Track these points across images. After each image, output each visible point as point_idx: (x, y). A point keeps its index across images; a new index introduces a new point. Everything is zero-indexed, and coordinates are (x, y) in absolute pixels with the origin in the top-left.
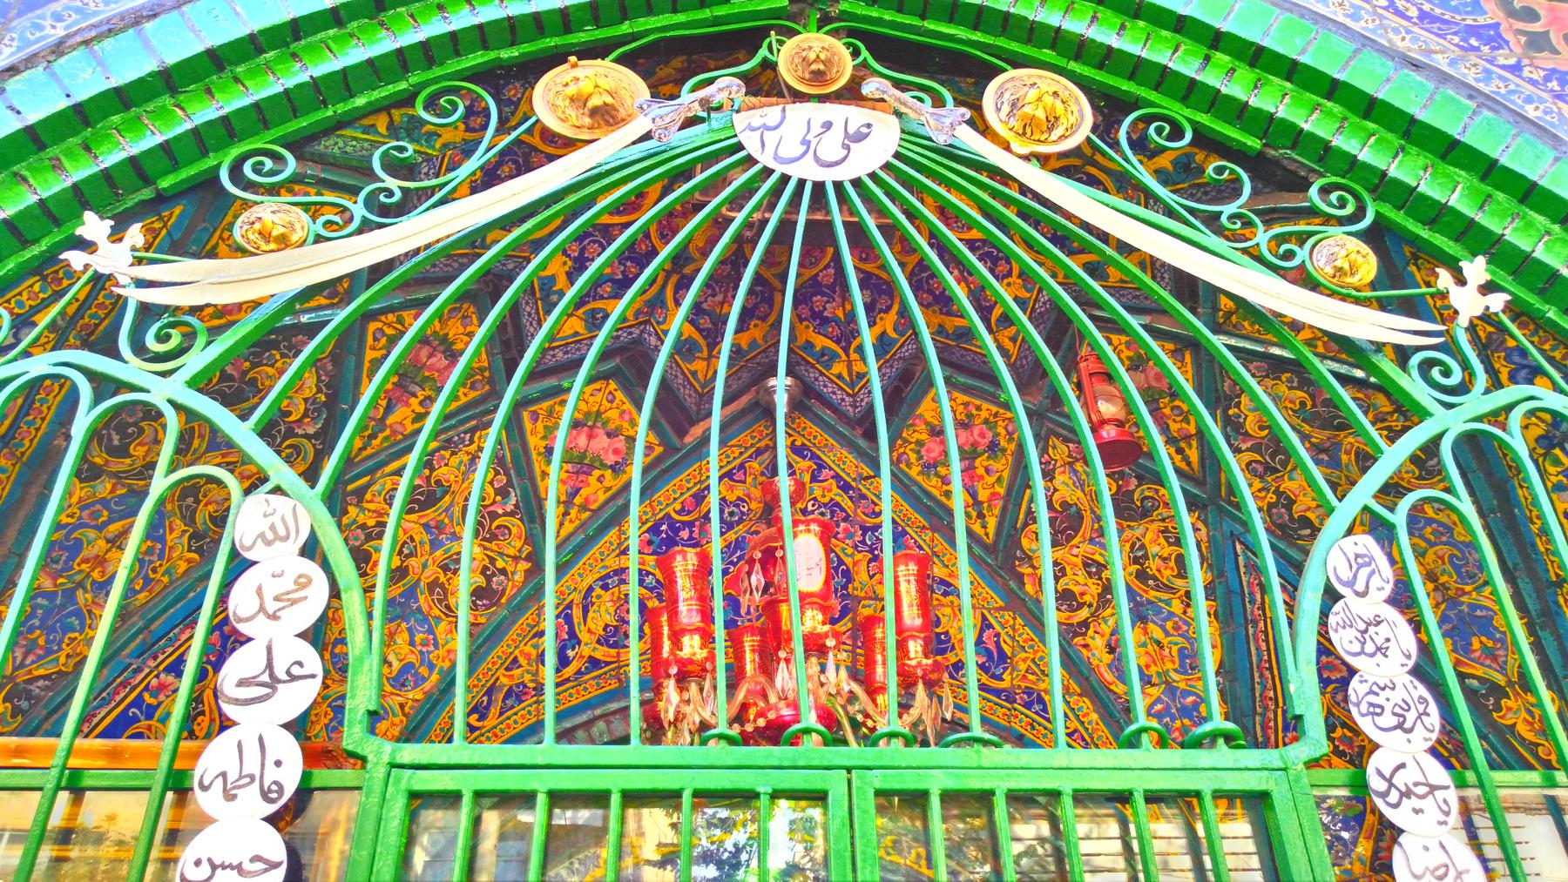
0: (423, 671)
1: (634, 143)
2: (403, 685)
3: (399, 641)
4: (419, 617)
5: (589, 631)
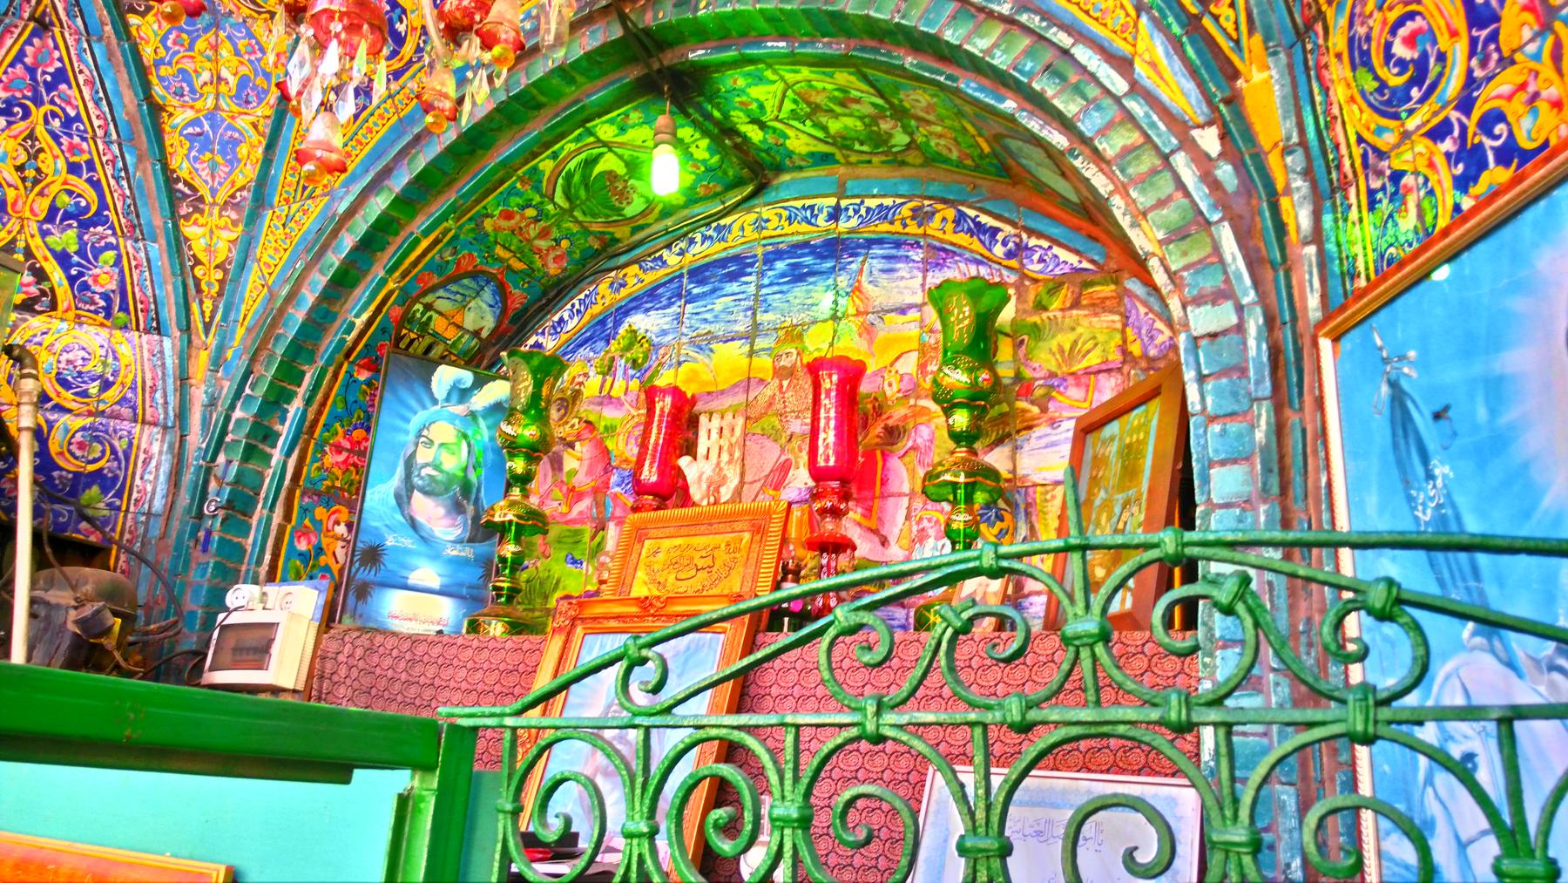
1: (1463, 685)
2: (247, 102)
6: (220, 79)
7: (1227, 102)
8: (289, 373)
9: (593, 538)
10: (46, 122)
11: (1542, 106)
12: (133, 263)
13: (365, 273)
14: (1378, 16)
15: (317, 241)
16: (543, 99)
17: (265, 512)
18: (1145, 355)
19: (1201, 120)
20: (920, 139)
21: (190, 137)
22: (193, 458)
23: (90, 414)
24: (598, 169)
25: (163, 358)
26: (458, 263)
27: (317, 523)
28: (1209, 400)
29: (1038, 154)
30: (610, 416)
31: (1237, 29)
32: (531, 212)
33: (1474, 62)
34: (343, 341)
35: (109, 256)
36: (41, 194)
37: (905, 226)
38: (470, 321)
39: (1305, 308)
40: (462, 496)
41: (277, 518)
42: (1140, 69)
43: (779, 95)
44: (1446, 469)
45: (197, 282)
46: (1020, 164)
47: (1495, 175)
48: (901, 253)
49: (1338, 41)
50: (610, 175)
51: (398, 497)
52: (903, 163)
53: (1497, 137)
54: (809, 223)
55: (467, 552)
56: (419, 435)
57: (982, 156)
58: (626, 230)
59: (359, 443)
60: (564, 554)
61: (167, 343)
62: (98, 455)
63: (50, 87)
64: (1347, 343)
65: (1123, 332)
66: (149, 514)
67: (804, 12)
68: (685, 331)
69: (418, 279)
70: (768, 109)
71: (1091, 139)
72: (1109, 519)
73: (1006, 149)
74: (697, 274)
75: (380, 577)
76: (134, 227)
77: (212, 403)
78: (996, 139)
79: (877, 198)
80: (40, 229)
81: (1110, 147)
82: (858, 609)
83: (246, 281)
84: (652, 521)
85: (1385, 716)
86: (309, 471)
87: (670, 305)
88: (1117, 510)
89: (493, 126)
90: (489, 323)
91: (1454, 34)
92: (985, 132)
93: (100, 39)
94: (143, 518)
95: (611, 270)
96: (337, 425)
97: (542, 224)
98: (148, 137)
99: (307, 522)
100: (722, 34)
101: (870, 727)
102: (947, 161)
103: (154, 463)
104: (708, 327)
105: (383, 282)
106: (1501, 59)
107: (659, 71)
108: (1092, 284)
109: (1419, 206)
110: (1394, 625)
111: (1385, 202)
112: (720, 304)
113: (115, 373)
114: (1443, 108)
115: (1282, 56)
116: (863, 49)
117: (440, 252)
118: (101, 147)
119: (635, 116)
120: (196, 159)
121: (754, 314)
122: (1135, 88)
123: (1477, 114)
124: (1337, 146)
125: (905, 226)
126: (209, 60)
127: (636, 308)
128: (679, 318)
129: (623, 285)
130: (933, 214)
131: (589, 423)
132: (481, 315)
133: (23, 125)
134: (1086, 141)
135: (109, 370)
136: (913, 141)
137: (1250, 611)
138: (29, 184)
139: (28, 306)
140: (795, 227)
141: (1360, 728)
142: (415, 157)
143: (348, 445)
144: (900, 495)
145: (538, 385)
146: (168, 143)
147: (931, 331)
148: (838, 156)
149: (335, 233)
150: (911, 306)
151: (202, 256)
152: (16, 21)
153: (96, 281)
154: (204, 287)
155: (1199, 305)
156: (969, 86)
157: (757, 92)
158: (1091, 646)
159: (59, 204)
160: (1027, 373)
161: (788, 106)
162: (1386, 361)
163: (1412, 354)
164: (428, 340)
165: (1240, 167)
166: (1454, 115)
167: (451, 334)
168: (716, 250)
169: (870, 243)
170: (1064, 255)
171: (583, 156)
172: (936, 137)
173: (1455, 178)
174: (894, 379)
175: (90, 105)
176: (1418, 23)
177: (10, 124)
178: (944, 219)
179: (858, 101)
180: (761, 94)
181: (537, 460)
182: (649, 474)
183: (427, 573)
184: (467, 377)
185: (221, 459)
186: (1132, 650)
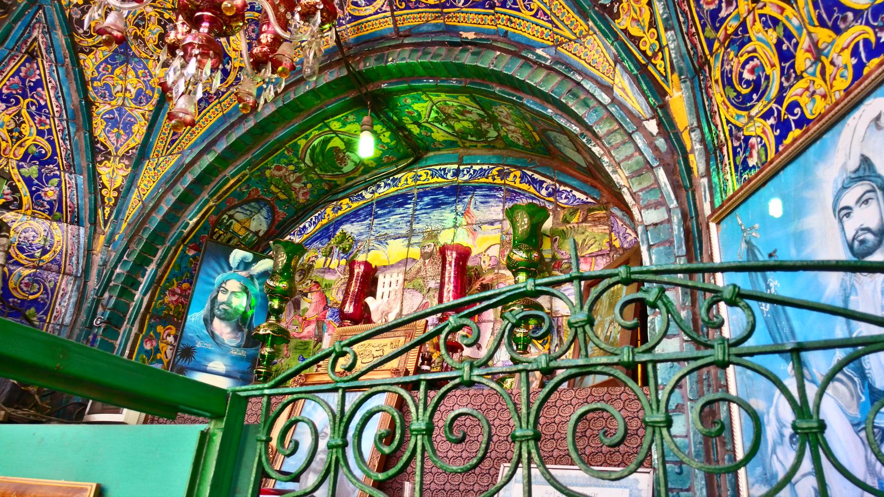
0: (149, 92)
2: (141, 103)
3: (130, 76)
4: (136, 59)
5: (234, 50)
6: (126, 89)
7: (661, 107)
8: (150, 249)
9: (315, 347)
10: (28, 107)
11: (817, 97)
12: (68, 186)
13: (197, 196)
14: (736, 60)
15: (172, 177)
16: (302, 107)
17: (129, 326)
18: (622, 247)
19: (648, 116)
20: (503, 134)
21: (107, 120)
22: (91, 294)
23: (34, 267)
24: (330, 145)
25: (79, 238)
26: (249, 194)
27: (158, 335)
28: (653, 257)
29: (564, 139)
30: (329, 278)
31: (665, 71)
32: (292, 168)
33: (783, 79)
34: (182, 232)
35: (55, 181)
36: (21, 146)
37: (494, 179)
38: (254, 225)
39: (703, 210)
40: (241, 323)
41: (135, 330)
42: (617, 91)
43: (429, 109)
44: (776, 283)
45: (103, 197)
46: (556, 147)
47: (795, 132)
48: (492, 193)
49: (717, 74)
50: (336, 149)
51: (205, 320)
52: (494, 147)
53: (795, 115)
54: (443, 177)
55: (243, 353)
56: (220, 286)
57: (536, 143)
58: (344, 179)
59: (185, 290)
60: (298, 355)
61: (82, 230)
62: (36, 290)
63: (32, 89)
64: (723, 225)
65: (610, 235)
66: (62, 325)
67: (443, 64)
68: (373, 233)
69: (227, 201)
70: (423, 116)
71: (592, 127)
72: (602, 331)
73: (548, 138)
74: (382, 203)
75: (191, 365)
76: (70, 166)
77: (105, 264)
78: (543, 133)
79: (479, 166)
80: (18, 165)
81: (601, 130)
82: (461, 317)
83: (131, 198)
84: (350, 331)
85: (737, 353)
86: (155, 305)
87: (364, 220)
88: (607, 326)
89: (275, 120)
90: (264, 228)
91: (773, 66)
92: (537, 129)
93: (62, 66)
94: (58, 327)
95: (334, 201)
96: (174, 279)
97: (298, 174)
98: (83, 117)
99: (151, 333)
100: (400, 75)
101: (466, 378)
102: (517, 146)
103: (67, 297)
104: (386, 231)
105: (207, 201)
106: (796, 76)
107: (366, 94)
108: (593, 210)
109: (758, 153)
110: (738, 309)
111: (741, 153)
112: (393, 219)
113: (51, 246)
114: (769, 103)
115: (688, 83)
116: (475, 84)
117: (240, 186)
118: (57, 122)
119: (351, 118)
120: (109, 131)
121: (411, 224)
122: (614, 101)
123: (785, 105)
124: (717, 126)
125: (494, 179)
126: (121, 79)
127: (347, 221)
128: (370, 227)
129: (340, 209)
130: (509, 174)
131: (316, 282)
132: (259, 223)
133: (14, 108)
134: (589, 128)
135: (48, 244)
136: (499, 135)
137: (665, 304)
138: (14, 140)
139: (6, 207)
140: (435, 179)
141: (721, 358)
142: (231, 134)
143: (179, 291)
144: (489, 321)
145: (289, 260)
146: (94, 122)
147: (507, 234)
148: (460, 143)
149: (183, 174)
150: (496, 221)
151: (107, 184)
152: (18, 53)
153: (46, 194)
154: (106, 201)
155: (648, 209)
156: (529, 102)
157: (417, 106)
158: (583, 326)
159: (30, 151)
160: (559, 256)
161: (433, 115)
162: (743, 231)
163: (757, 226)
164: (229, 235)
165: (668, 139)
166: (774, 106)
167: (242, 233)
168: (391, 191)
169: (475, 188)
170: (578, 195)
171: (322, 138)
172: (513, 132)
173: (775, 136)
174: (486, 259)
175: (53, 100)
176: (756, 61)
177: (7, 107)
178: (515, 176)
179: (470, 112)
180: (420, 108)
181: (287, 301)
182: (349, 309)
183: (219, 364)
184: (249, 256)
185: (106, 295)
186: (615, 397)
